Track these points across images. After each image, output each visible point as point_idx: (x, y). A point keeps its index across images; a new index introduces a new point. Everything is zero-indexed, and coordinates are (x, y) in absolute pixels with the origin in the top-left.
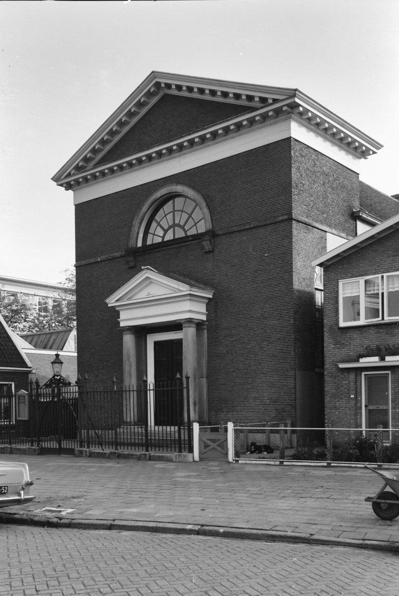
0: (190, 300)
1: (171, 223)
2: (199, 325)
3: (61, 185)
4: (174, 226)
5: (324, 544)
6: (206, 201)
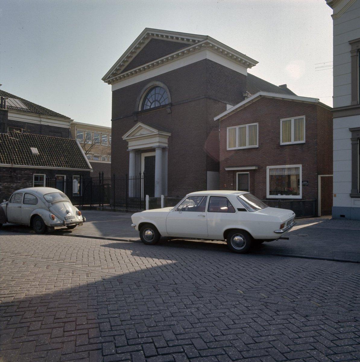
0: (159, 137)
1: (154, 100)
2: (164, 149)
3: (106, 82)
4: (155, 101)
5: (6, 303)
6: (169, 89)
